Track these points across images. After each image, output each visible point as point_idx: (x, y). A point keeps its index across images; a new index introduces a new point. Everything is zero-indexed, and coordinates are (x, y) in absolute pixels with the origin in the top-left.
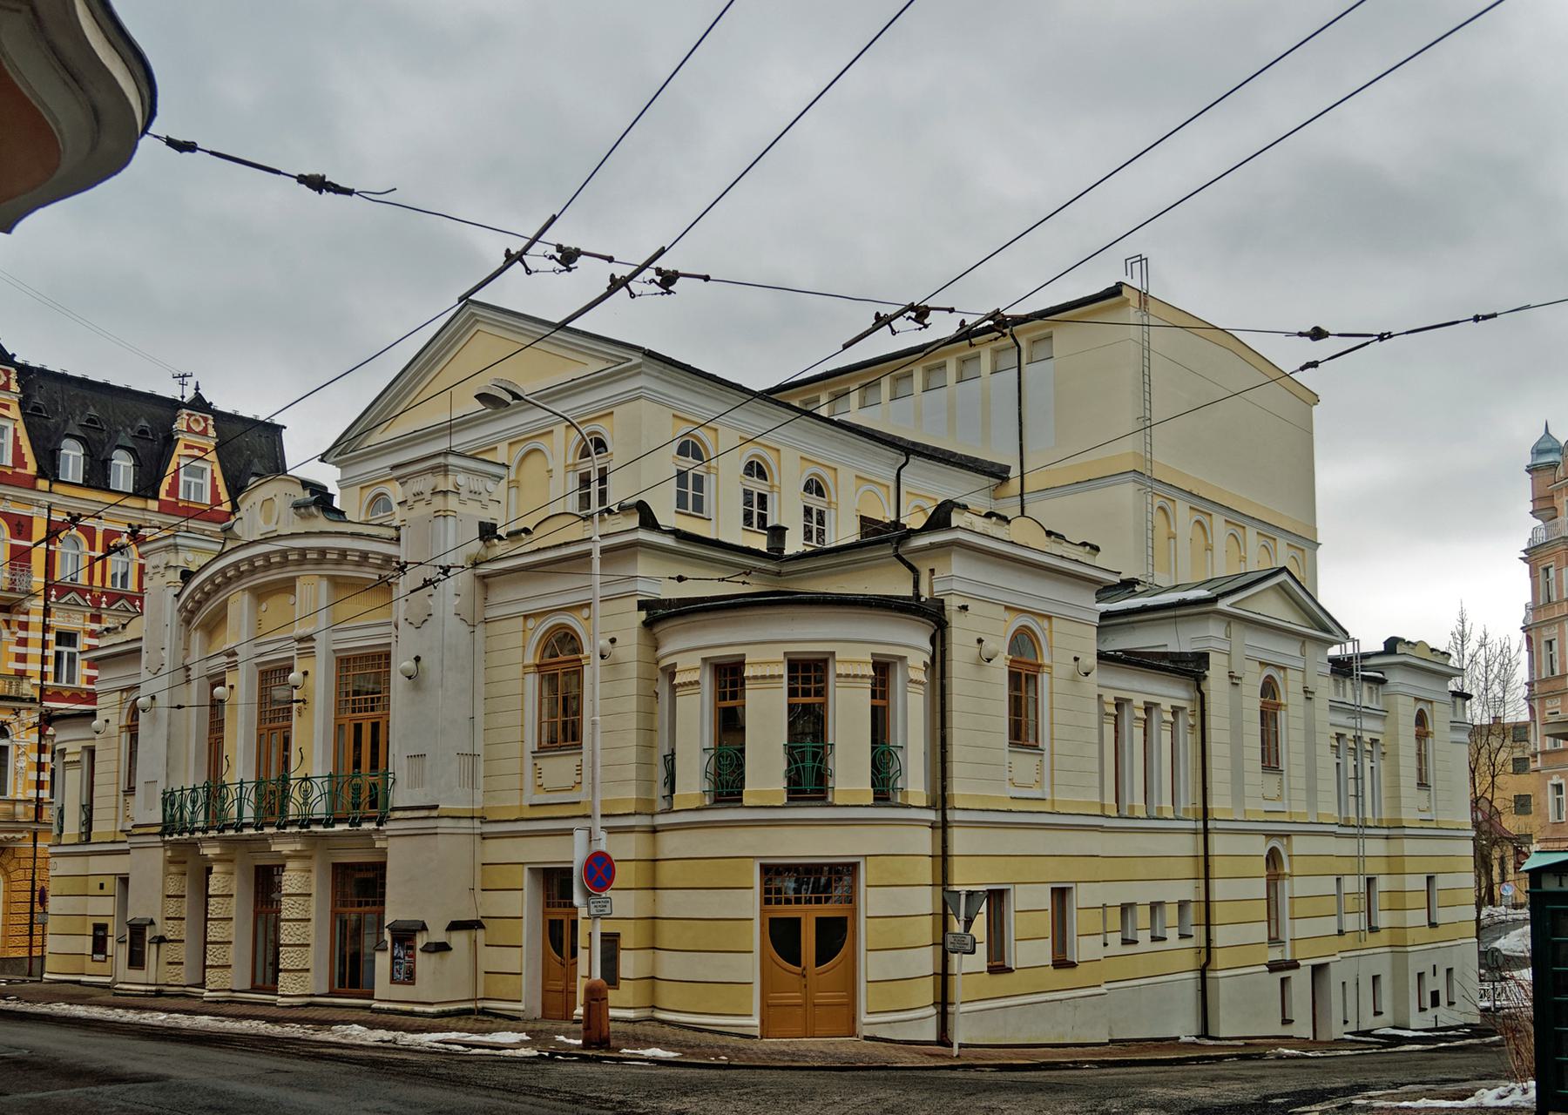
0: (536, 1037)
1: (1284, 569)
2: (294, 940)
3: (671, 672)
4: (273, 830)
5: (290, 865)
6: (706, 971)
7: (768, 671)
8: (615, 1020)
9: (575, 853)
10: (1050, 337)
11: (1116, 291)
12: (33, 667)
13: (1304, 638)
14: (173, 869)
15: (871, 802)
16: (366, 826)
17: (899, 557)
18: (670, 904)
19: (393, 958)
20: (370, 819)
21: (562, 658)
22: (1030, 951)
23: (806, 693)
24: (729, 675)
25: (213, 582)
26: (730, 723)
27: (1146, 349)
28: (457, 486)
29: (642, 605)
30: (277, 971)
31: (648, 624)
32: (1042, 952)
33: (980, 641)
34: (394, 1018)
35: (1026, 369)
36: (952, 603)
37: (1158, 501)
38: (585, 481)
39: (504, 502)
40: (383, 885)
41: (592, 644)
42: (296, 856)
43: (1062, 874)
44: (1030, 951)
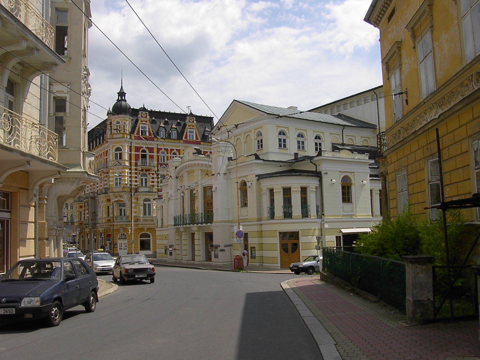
12: (156, 184)
14: (177, 233)
15: (301, 218)
17: (311, 162)
25: (184, 167)
26: (272, 201)
28: (222, 150)
29: (256, 176)
30: (195, 256)
36: (323, 172)
41: (248, 184)
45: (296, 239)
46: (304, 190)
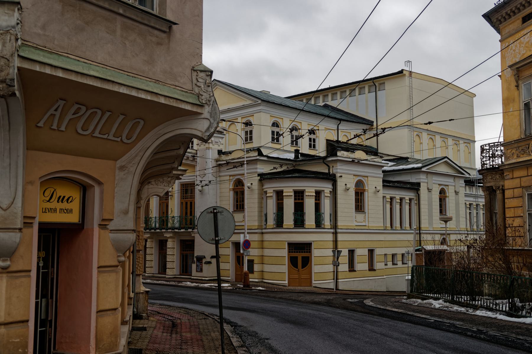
0: (232, 285)
1: (446, 157)
2: (170, 260)
3: (266, 193)
4: (164, 230)
5: (169, 240)
6: (276, 270)
7: (289, 194)
8: (251, 282)
9: (241, 239)
10: (384, 83)
11: (401, 72)
13: (455, 177)
16: (189, 230)
18: (267, 252)
19: (197, 265)
20: (190, 228)
21: (239, 187)
22: (362, 266)
23: (299, 199)
24: (279, 194)
27: (411, 87)
29: (259, 175)
31: (260, 180)
32: (366, 266)
33: (346, 185)
34: (197, 281)
35: (378, 93)
36: (338, 175)
37: (415, 133)
38: (246, 132)
39: (224, 144)
40: (194, 246)
41: (247, 184)
42: (171, 237)
43: (371, 246)
44: (362, 266)
45: (307, 252)
46: (318, 194)
